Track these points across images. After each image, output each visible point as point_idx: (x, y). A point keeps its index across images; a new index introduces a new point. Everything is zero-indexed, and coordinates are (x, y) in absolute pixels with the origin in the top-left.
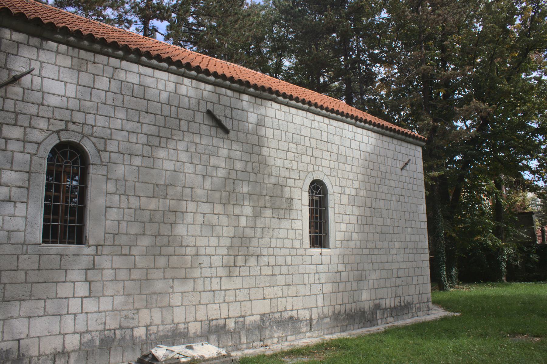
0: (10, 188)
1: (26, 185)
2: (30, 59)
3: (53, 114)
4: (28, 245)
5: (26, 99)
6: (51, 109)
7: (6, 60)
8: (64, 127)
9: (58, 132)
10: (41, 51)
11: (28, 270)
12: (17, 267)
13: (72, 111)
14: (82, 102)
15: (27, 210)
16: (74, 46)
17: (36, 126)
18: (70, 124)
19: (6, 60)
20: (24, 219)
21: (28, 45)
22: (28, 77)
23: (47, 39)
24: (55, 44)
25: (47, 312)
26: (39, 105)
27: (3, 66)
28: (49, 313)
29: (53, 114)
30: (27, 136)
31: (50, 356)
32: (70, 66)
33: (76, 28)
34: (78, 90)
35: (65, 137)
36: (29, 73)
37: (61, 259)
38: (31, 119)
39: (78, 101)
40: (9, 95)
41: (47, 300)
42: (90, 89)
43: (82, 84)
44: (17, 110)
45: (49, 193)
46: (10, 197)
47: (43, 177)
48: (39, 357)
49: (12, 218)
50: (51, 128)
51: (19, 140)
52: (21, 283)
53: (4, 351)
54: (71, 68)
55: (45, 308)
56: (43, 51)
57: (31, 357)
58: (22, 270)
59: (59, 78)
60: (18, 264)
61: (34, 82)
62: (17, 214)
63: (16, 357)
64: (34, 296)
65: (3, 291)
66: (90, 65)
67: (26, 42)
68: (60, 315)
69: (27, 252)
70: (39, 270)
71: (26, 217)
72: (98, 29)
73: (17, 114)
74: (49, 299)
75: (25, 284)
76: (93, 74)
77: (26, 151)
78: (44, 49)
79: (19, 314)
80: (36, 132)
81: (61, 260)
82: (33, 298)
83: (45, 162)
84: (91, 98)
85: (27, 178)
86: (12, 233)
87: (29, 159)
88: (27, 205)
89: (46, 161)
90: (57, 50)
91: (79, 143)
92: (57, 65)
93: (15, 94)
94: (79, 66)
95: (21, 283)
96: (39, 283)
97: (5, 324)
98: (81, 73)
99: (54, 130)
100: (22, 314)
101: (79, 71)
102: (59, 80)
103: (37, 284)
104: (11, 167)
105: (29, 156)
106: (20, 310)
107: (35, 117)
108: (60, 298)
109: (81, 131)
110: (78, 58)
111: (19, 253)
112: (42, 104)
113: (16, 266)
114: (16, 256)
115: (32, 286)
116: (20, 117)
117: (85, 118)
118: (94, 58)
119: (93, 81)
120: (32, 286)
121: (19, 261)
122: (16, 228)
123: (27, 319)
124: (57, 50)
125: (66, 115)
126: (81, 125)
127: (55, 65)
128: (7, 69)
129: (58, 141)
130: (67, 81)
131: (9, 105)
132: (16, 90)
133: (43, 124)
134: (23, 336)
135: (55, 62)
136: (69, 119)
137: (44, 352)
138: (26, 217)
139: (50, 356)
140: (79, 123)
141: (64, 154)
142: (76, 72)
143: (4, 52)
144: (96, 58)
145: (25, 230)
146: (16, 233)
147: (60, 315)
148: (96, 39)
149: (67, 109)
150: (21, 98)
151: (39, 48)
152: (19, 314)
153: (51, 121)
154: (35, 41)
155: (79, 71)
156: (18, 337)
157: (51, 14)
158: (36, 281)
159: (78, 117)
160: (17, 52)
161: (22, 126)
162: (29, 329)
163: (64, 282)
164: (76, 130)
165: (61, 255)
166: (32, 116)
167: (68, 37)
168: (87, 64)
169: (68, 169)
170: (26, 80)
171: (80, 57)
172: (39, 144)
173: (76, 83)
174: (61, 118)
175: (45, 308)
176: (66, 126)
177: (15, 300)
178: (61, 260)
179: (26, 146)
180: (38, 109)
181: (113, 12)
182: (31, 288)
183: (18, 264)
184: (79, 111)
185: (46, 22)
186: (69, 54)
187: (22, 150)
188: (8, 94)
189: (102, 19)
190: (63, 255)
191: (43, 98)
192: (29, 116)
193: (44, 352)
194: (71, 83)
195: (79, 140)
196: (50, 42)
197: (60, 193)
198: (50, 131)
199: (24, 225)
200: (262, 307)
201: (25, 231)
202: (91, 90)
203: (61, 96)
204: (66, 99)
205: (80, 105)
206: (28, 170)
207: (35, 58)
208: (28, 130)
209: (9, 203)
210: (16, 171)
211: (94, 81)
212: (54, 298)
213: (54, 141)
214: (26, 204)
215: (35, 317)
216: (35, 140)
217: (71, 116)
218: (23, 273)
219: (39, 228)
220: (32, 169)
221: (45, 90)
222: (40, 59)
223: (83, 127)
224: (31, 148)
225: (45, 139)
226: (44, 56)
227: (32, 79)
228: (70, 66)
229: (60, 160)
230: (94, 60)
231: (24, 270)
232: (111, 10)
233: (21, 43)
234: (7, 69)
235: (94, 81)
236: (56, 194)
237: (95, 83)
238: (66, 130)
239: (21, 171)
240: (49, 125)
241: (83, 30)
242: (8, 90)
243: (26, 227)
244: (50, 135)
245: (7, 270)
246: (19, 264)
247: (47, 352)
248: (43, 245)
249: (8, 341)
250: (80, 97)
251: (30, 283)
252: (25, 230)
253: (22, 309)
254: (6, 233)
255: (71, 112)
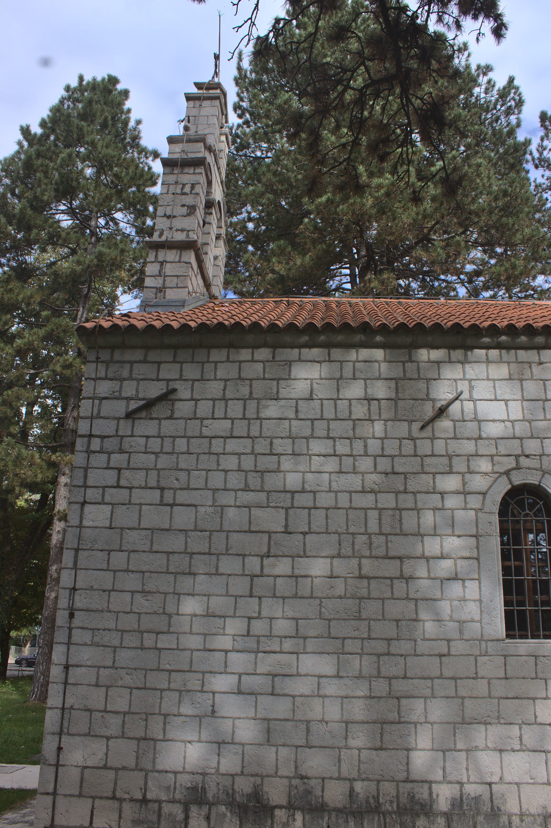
0: (455, 561)
1: (475, 555)
2: (455, 380)
3: (497, 449)
4: (487, 641)
5: (459, 435)
6: (493, 442)
7: (428, 388)
8: (514, 465)
9: (507, 473)
10: (467, 366)
11: (491, 678)
12: (476, 673)
13: (521, 439)
14: (533, 423)
15: (480, 591)
16: (508, 348)
17: (477, 469)
18: (522, 459)
19: (428, 388)
20: (478, 603)
21: (450, 362)
22: (457, 404)
23: (472, 348)
24: (483, 352)
25: (525, 746)
26: (476, 439)
27: (425, 397)
28: (528, 746)
29: (497, 449)
30: (467, 486)
31: (537, 818)
32: (507, 377)
33: (505, 323)
34: (525, 407)
35: (518, 479)
36: (457, 399)
37: (536, 662)
38: (468, 461)
39: (527, 424)
40: (437, 435)
41: (523, 726)
42: (541, 402)
43: (529, 398)
44: (450, 452)
45: (507, 563)
46: (456, 574)
47: (496, 540)
48: (522, 815)
49: (462, 602)
50: (496, 469)
51: (457, 493)
52: (484, 698)
53: (472, 798)
54: (510, 379)
55: (521, 738)
56: (470, 365)
57: (510, 816)
58: (482, 678)
59: (495, 396)
60: (476, 669)
61: (466, 410)
62: (467, 597)
63: (489, 810)
64: (503, 718)
65: (461, 708)
66: (535, 369)
67: (447, 360)
68: (544, 751)
69: (486, 652)
70: (506, 678)
71: (480, 601)
72: (534, 313)
73: (450, 457)
74: (526, 724)
75: (489, 700)
76: (541, 380)
77: (468, 507)
78: (470, 363)
79: (486, 744)
80: (478, 477)
81: (536, 665)
82: (502, 721)
83: (496, 519)
84: (545, 416)
85: (475, 544)
86: (464, 624)
87: (474, 517)
88: (480, 583)
89: (497, 517)
90: (487, 359)
91: (539, 485)
92: (491, 380)
93: (445, 431)
94: (521, 373)
95: (484, 698)
96: (508, 698)
97: (469, 757)
98: (524, 382)
99: (502, 470)
100: (490, 745)
101: (521, 380)
102: (496, 400)
103: (506, 701)
104: (453, 531)
105: (473, 513)
106: (486, 738)
107: (474, 458)
108: (541, 724)
109: (539, 466)
110: (517, 362)
111: (476, 654)
112: (480, 438)
113: (474, 672)
114: (473, 657)
115: (499, 703)
116: (455, 460)
117: (543, 447)
118: (539, 356)
119: (543, 391)
120: (499, 703)
121: (478, 665)
122: (469, 617)
123: (497, 754)
124: (487, 359)
125: (514, 447)
126: (538, 457)
127: (488, 379)
128: (431, 400)
129: (509, 487)
130: (507, 398)
131: (440, 446)
132: (445, 424)
133: (485, 465)
134: (495, 779)
135: (488, 375)
136: (519, 452)
137: (528, 809)
138: (480, 601)
139: (537, 818)
140: (535, 455)
141: (521, 504)
142: (517, 384)
143: (423, 379)
144: (541, 356)
145: (481, 620)
146: (470, 624)
147: (544, 751)
148: (537, 329)
149: (514, 438)
150: (452, 435)
151: (464, 362)
152: (486, 744)
153: (496, 458)
154: (458, 354)
155: (521, 380)
156: (489, 780)
157: (469, 311)
158: (504, 695)
159: (532, 446)
160: (439, 374)
161: (459, 473)
162: (502, 768)
163: (545, 699)
164: (532, 466)
165: (536, 657)
166: (469, 457)
167: (498, 338)
168: (530, 367)
169: (528, 525)
170: (455, 408)
171: (519, 360)
172: (484, 494)
173: (520, 398)
174: (508, 453)
175: (521, 738)
176: (517, 462)
177: (478, 723)
178: (536, 665)
179: (468, 500)
180: (476, 445)
181: (546, 278)
182: (499, 706)
183: (476, 669)
184: (532, 437)
185: (466, 325)
186: (504, 360)
187: (463, 506)
188: (435, 433)
189: (532, 292)
190: (539, 656)
191: (480, 429)
192: (466, 457)
193: (528, 809)
194: (514, 400)
195: (539, 480)
196: (476, 350)
197: (522, 561)
198: (496, 473)
199: (479, 611)
200: (435, 505)
201: (480, 621)
202: (544, 404)
203: (503, 421)
204: (510, 424)
205: (531, 429)
206: (475, 533)
207: (462, 377)
208: (467, 476)
209: (456, 581)
210: (459, 536)
211: (545, 390)
212: (532, 724)
213: (503, 487)
214: (477, 581)
215: (508, 750)
216: (478, 489)
217: (522, 446)
218: (485, 681)
219: (499, 616)
220: (480, 531)
221: (480, 417)
222: (467, 377)
223: (541, 460)
224: (474, 501)
225: (491, 486)
226: (471, 371)
227: (462, 405)
228: (507, 377)
229: (516, 512)
230: (540, 360)
231: (485, 678)
232: (543, 276)
233: (441, 362)
234: (431, 400)
235: (545, 390)
236: (517, 563)
237: (548, 392)
238: (518, 468)
239: (466, 536)
240: (493, 465)
241: (516, 321)
242: (435, 428)
243: (481, 615)
244: (497, 478)
245: (463, 678)
246: (478, 669)
247: (533, 811)
248: (507, 641)
249: (475, 783)
250: (530, 417)
251: (496, 698)
252: (481, 620)
253: (489, 736)
254: (456, 624)
255: (521, 442)
